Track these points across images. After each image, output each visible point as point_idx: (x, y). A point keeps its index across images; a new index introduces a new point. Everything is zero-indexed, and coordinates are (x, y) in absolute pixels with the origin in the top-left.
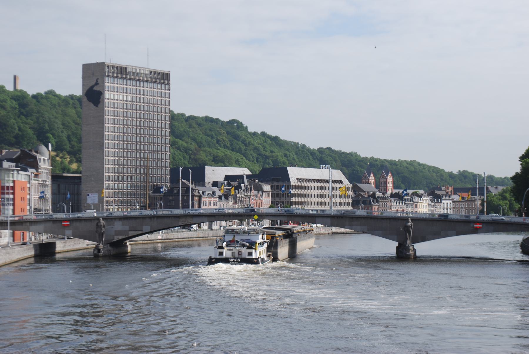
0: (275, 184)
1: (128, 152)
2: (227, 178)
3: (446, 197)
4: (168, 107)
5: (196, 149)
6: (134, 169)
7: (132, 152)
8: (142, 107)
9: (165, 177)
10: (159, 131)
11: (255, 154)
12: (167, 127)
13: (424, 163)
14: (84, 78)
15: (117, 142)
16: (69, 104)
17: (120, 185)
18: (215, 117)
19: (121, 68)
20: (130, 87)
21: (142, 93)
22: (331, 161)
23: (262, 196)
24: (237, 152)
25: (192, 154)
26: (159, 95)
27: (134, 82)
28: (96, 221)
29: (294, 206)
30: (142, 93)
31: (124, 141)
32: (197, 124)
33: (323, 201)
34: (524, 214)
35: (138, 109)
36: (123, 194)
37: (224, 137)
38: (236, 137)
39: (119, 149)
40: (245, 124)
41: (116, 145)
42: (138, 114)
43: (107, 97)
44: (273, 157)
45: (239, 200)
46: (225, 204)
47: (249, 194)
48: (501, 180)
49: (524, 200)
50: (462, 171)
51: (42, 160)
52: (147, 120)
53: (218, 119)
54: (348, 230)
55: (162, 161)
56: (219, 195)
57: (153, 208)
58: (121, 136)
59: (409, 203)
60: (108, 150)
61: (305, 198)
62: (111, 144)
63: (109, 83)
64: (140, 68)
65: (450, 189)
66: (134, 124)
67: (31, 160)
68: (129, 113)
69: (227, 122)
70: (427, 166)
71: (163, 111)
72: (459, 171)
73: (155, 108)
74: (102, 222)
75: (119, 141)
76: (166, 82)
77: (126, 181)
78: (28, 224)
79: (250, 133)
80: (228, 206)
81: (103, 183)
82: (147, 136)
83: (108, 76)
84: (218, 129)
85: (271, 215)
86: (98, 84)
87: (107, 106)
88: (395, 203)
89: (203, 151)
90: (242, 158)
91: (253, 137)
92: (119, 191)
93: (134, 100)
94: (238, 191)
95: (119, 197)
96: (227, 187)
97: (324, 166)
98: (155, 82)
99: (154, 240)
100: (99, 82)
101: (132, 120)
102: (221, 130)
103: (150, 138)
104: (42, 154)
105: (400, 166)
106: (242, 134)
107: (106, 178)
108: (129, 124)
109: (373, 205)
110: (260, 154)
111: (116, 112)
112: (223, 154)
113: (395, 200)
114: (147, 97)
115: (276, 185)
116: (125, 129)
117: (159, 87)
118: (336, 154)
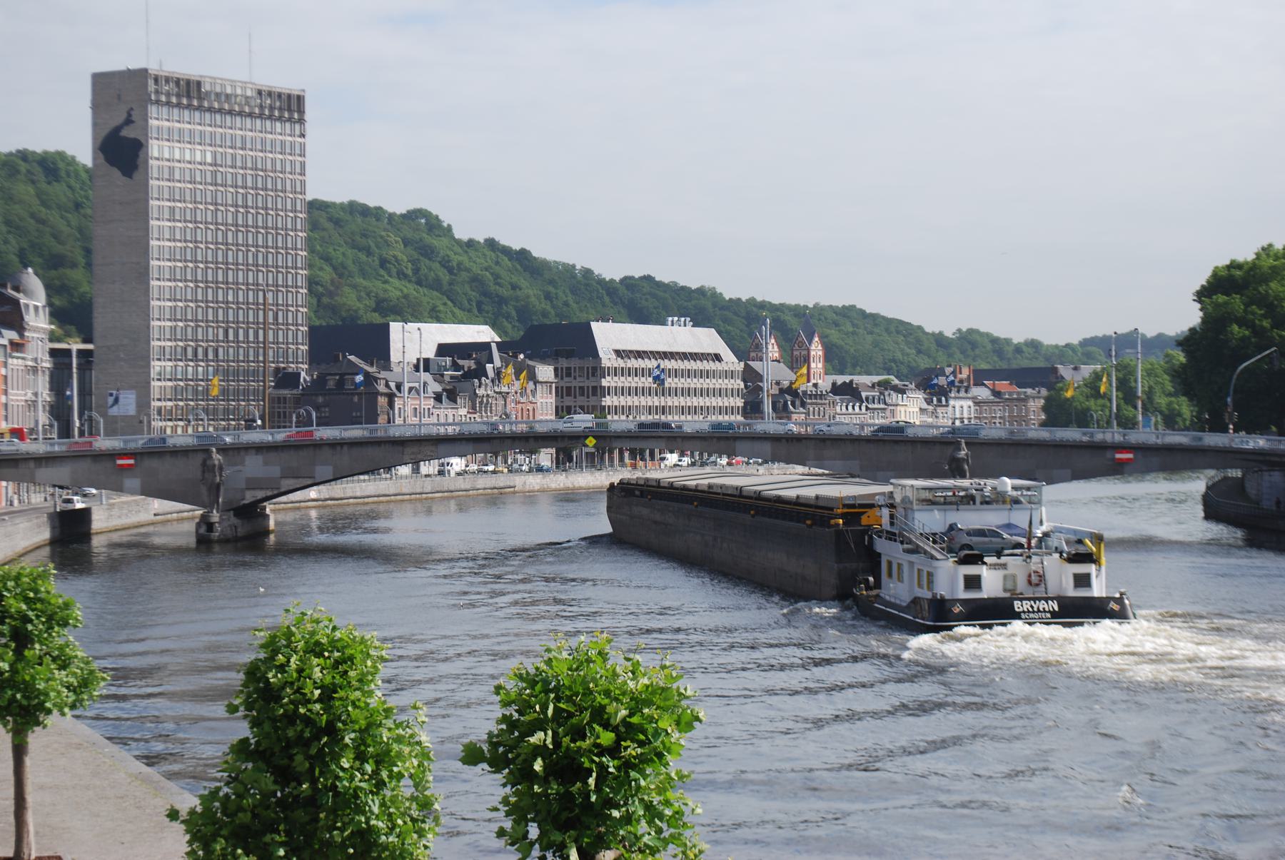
0: (564, 363)
1: (207, 287)
2: (443, 349)
3: (958, 392)
4: (300, 177)
5: (332, 281)
6: (221, 331)
7: (218, 288)
8: (239, 177)
9: (297, 349)
10: (280, 238)
11: (474, 293)
12: (299, 227)
13: (874, 312)
14: (96, 106)
15: (179, 264)
16: (18, 172)
17: (190, 369)
18: (372, 203)
19: (188, 82)
20: (209, 129)
21: (239, 144)
22: (655, 308)
23: (534, 392)
24: (431, 287)
25: (322, 295)
26: (278, 149)
27: (218, 117)
28: (199, 458)
29: (609, 417)
30: (239, 144)
31: (196, 261)
32: (330, 219)
33: (676, 404)
34: (1231, 426)
35: (229, 182)
36: (196, 392)
37: (398, 251)
38: (427, 252)
39: (186, 281)
40: (446, 219)
41: (178, 270)
42: (229, 195)
43: (156, 154)
44: (517, 299)
45: (481, 403)
46: (450, 413)
47: (505, 389)
48: (1057, 351)
49: (1231, 392)
50: (964, 330)
51: (32, 310)
52: (252, 211)
53: (380, 208)
54: (826, 472)
55: (287, 311)
56: (434, 393)
57: (276, 424)
58: (189, 251)
59: (876, 406)
60: (158, 283)
61: (636, 398)
62: (167, 270)
63: (158, 120)
64: (233, 83)
65: (965, 373)
66: (220, 221)
67: (6, 308)
68: (209, 193)
69: (403, 216)
70: (883, 317)
71: (288, 188)
72: (959, 330)
73: (269, 180)
74: (217, 458)
75: (186, 261)
76: (296, 116)
77: (202, 361)
78: (32, 464)
79: (459, 242)
80: (454, 417)
81: (148, 366)
82: (253, 249)
83: (158, 102)
84: (383, 233)
85: (626, 437)
86: (132, 122)
87: (155, 175)
88: (844, 408)
89: (349, 285)
90: (445, 304)
91: (466, 252)
92: (187, 385)
93: (219, 162)
94: (480, 380)
95: (186, 400)
96: (450, 373)
97: (676, 319)
98: (270, 117)
99: (300, 502)
100: (134, 118)
101: (217, 210)
102: (388, 236)
103: (260, 255)
104: (28, 293)
105: (819, 320)
106: (439, 243)
107: (154, 354)
108: (209, 220)
109: (792, 413)
110: (485, 294)
111: (177, 191)
112: (398, 293)
113: (842, 401)
114: (251, 153)
115: (565, 365)
116: (199, 231)
117: (279, 130)
118: (665, 292)
